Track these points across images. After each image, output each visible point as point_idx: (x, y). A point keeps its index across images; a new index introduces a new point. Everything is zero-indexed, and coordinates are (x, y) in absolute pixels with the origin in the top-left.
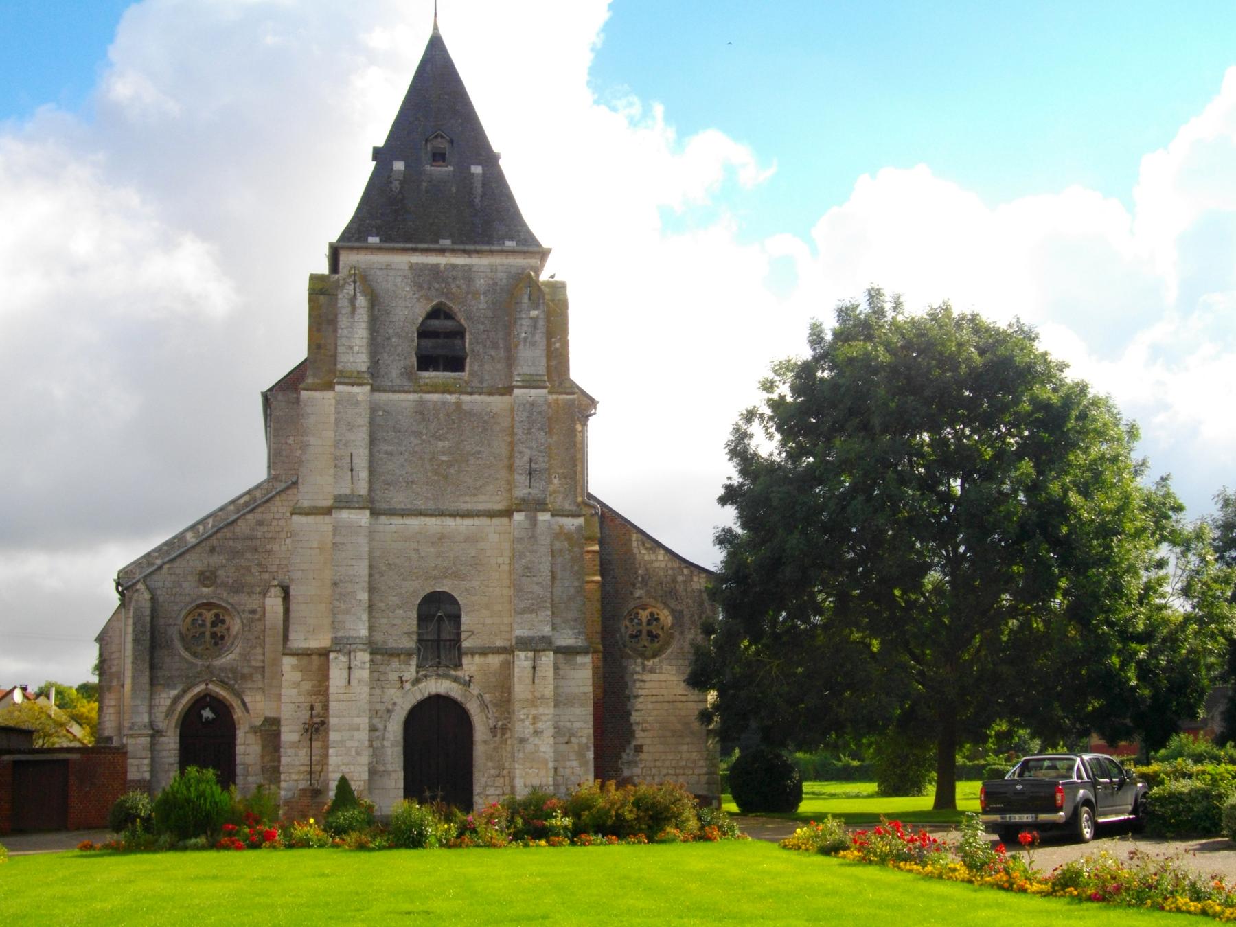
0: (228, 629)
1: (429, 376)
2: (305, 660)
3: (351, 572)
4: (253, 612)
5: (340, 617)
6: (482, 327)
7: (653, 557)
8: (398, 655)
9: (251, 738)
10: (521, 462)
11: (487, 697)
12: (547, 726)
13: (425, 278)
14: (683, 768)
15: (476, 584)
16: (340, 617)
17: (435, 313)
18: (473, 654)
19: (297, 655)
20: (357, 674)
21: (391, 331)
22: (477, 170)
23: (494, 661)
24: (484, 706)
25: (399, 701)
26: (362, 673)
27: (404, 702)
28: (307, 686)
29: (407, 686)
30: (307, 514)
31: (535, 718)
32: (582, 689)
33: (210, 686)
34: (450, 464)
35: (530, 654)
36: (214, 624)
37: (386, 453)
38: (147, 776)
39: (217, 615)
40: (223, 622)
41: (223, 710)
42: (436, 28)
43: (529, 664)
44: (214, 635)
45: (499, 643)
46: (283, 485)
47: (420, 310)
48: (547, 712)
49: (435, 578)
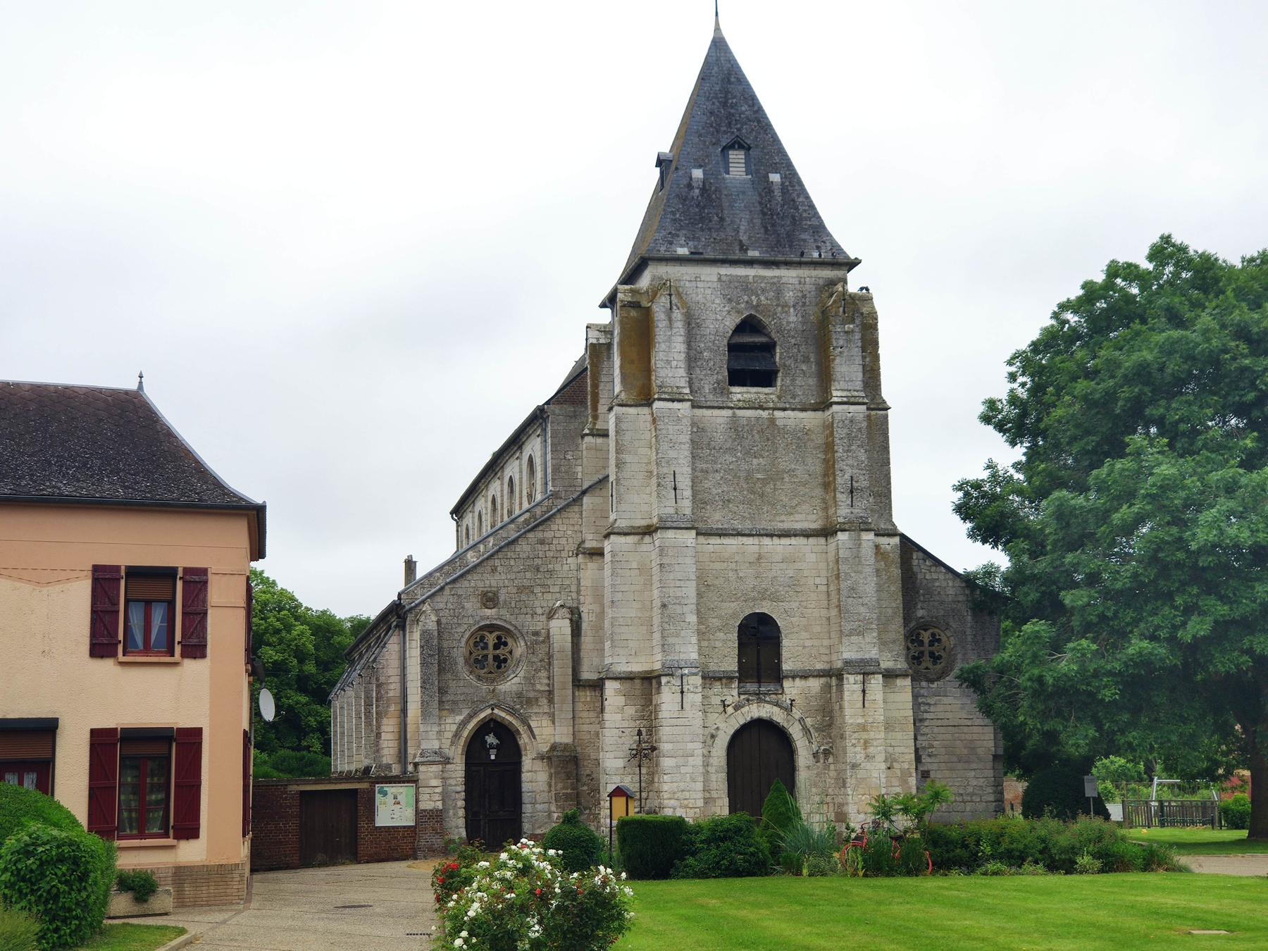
0: (511, 652)
1: (739, 393)
2: (628, 684)
3: (679, 594)
4: (536, 634)
5: (671, 640)
6: (793, 341)
7: (935, 576)
8: (720, 679)
9: (539, 765)
10: (842, 480)
11: (809, 721)
12: (878, 751)
13: (731, 290)
14: (972, 794)
15: (794, 605)
16: (671, 640)
17: (741, 328)
18: (794, 677)
19: (620, 679)
20: (689, 698)
21: (702, 345)
22: (775, 178)
23: (815, 684)
24: (806, 730)
25: (722, 725)
26: (694, 698)
27: (728, 727)
28: (631, 711)
29: (730, 710)
30: (626, 534)
31: (866, 742)
32: (903, 713)
33: (496, 711)
34: (765, 482)
35: (860, 677)
36: (496, 647)
37: (702, 471)
38: (439, 805)
39: (499, 638)
40: (505, 644)
41: (507, 736)
42: (717, 28)
43: (859, 687)
44: (496, 658)
45: (819, 666)
46: (562, 503)
47: (731, 322)
48: (878, 735)
49: (754, 599)
